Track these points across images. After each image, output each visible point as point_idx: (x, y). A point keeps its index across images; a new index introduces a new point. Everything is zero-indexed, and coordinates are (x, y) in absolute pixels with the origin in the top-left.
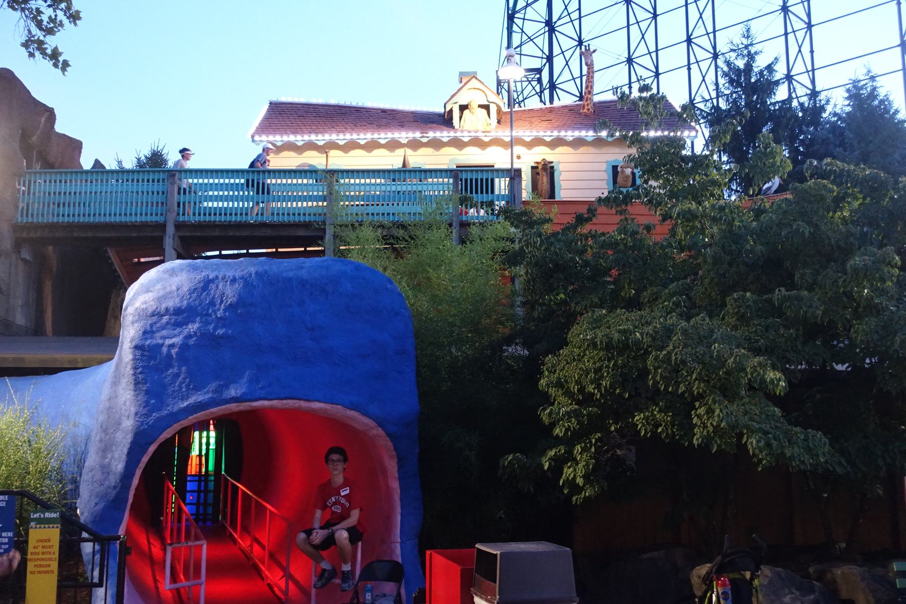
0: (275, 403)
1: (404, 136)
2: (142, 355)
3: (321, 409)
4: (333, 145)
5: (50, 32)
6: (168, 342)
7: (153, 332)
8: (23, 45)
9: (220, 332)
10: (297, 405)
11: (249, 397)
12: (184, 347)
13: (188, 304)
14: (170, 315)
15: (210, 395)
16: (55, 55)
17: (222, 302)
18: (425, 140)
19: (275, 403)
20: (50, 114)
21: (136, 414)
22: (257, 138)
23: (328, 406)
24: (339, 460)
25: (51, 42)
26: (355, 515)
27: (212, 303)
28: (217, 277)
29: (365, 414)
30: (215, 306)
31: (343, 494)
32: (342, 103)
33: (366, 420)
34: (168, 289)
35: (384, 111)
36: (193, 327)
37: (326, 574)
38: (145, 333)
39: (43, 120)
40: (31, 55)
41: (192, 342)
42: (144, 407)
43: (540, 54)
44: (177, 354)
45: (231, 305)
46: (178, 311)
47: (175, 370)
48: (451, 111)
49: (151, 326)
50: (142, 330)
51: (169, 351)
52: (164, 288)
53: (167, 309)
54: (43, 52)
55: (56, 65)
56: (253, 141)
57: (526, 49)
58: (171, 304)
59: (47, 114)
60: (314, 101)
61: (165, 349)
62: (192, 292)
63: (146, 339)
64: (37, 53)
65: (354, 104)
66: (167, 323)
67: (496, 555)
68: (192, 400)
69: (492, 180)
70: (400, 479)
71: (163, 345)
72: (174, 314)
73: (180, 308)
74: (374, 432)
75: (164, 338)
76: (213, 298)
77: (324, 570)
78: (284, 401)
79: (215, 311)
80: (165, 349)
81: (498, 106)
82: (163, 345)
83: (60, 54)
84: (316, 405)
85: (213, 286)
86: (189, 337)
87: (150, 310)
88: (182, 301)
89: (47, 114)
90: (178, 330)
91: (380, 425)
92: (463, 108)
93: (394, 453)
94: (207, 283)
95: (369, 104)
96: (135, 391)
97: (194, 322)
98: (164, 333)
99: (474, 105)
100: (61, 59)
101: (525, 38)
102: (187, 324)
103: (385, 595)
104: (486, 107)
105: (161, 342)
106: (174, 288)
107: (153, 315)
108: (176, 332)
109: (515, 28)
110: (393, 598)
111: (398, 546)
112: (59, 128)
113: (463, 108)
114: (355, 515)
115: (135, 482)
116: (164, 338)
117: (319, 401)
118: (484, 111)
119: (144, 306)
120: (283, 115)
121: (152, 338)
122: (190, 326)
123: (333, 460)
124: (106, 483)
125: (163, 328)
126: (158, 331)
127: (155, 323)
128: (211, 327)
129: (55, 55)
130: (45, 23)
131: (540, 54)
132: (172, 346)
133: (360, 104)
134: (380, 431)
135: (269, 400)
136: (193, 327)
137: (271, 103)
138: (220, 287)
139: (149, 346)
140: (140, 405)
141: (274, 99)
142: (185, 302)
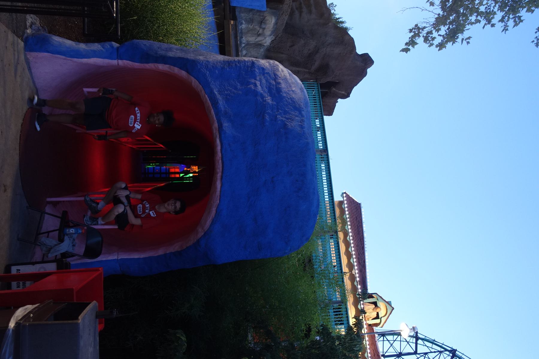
0: (219, 154)
1: (356, 271)
2: (248, 67)
3: (216, 188)
4: (346, 234)
5: (426, 39)
6: (258, 83)
7: (263, 74)
8: (416, 25)
9: (267, 117)
10: (218, 170)
11: (223, 135)
12: (256, 93)
13: (284, 97)
14: (276, 85)
15: (223, 109)
16: (412, 43)
17: (288, 119)
18: (355, 283)
19: (219, 154)
20: (346, 96)
21: (208, 61)
22: (344, 195)
23: (218, 193)
24: (176, 207)
25: (420, 40)
26: (137, 222)
27: (285, 112)
28: (303, 116)
29: (213, 222)
30: (284, 114)
31: (151, 212)
32: (365, 240)
33: (209, 223)
34: (293, 86)
35: (364, 262)
36: (269, 99)
37: (94, 205)
38: (263, 69)
39: (343, 92)
40: (411, 31)
41: (259, 98)
42: (213, 67)
43: (385, 351)
44: (250, 88)
45: (286, 125)
46: (279, 90)
47: (239, 87)
48: (373, 297)
49: (268, 73)
50: (265, 67)
51: (252, 83)
52: (293, 83)
53: (280, 83)
54: (413, 37)
55: (406, 44)
56: (343, 194)
57: (386, 343)
58: (283, 85)
59: (346, 94)
60: (364, 225)
61: (253, 81)
62: (292, 99)
63: (259, 69)
64: (412, 34)
65: (366, 246)
66: (270, 83)
67: (77, 318)
68: (219, 97)
69: (343, 324)
70: (165, 255)
71: (256, 79)
72: (276, 88)
73: (281, 91)
74: (200, 230)
75: (260, 81)
76: (290, 114)
77: (98, 204)
78: (220, 161)
79: (280, 114)
80: (253, 81)
81: (379, 324)
82: (256, 79)
83: (413, 47)
84: (219, 185)
85: (297, 113)
86: (263, 97)
87: (278, 73)
88: (285, 93)
89: (346, 94)
90: (266, 90)
91: (206, 233)
92: (375, 304)
93: (185, 247)
94: (298, 109)
95: (367, 254)
96: (224, 61)
97: (272, 100)
98: (264, 81)
99: (378, 310)
100: (410, 47)
101: (392, 342)
102: (271, 96)
103: (74, 246)
104: (377, 317)
105: (258, 78)
106: (294, 89)
107: (275, 75)
108: (265, 88)
109: (395, 337)
110: (71, 250)
111: (116, 257)
112: (339, 100)
113: (375, 304)
114: (137, 222)
115: (162, 67)
116: (260, 81)
117: (221, 187)
118: (375, 316)
119: (280, 70)
120: (356, 208)
121: (260, 73)
122: (269, 98)
123: (175, 203)
124: (159, 50)
125: (267, 81)
126: (265, 77)
127: (270, 76)
128: (269, 111)
129: (412, 43)
130: (431, 36)
131: (385, 351)
132: (255, 85)
133: (366, 249)
134: (201, 234)
135: (221, 150)
136: (269, 99)
137: (360, 204)
138: (297, 118)
139: (255, 71)
140: (214, 64)
141: (362, 205)
142: (285, 95)
